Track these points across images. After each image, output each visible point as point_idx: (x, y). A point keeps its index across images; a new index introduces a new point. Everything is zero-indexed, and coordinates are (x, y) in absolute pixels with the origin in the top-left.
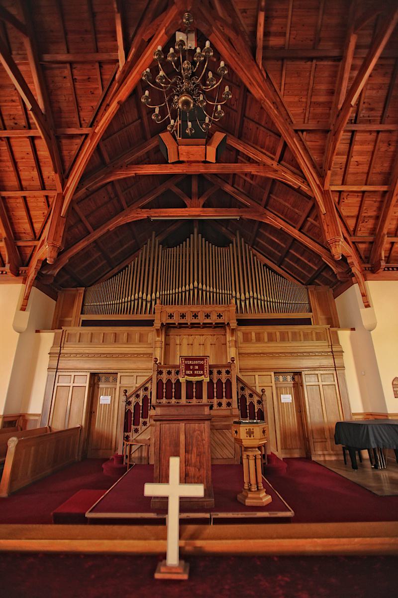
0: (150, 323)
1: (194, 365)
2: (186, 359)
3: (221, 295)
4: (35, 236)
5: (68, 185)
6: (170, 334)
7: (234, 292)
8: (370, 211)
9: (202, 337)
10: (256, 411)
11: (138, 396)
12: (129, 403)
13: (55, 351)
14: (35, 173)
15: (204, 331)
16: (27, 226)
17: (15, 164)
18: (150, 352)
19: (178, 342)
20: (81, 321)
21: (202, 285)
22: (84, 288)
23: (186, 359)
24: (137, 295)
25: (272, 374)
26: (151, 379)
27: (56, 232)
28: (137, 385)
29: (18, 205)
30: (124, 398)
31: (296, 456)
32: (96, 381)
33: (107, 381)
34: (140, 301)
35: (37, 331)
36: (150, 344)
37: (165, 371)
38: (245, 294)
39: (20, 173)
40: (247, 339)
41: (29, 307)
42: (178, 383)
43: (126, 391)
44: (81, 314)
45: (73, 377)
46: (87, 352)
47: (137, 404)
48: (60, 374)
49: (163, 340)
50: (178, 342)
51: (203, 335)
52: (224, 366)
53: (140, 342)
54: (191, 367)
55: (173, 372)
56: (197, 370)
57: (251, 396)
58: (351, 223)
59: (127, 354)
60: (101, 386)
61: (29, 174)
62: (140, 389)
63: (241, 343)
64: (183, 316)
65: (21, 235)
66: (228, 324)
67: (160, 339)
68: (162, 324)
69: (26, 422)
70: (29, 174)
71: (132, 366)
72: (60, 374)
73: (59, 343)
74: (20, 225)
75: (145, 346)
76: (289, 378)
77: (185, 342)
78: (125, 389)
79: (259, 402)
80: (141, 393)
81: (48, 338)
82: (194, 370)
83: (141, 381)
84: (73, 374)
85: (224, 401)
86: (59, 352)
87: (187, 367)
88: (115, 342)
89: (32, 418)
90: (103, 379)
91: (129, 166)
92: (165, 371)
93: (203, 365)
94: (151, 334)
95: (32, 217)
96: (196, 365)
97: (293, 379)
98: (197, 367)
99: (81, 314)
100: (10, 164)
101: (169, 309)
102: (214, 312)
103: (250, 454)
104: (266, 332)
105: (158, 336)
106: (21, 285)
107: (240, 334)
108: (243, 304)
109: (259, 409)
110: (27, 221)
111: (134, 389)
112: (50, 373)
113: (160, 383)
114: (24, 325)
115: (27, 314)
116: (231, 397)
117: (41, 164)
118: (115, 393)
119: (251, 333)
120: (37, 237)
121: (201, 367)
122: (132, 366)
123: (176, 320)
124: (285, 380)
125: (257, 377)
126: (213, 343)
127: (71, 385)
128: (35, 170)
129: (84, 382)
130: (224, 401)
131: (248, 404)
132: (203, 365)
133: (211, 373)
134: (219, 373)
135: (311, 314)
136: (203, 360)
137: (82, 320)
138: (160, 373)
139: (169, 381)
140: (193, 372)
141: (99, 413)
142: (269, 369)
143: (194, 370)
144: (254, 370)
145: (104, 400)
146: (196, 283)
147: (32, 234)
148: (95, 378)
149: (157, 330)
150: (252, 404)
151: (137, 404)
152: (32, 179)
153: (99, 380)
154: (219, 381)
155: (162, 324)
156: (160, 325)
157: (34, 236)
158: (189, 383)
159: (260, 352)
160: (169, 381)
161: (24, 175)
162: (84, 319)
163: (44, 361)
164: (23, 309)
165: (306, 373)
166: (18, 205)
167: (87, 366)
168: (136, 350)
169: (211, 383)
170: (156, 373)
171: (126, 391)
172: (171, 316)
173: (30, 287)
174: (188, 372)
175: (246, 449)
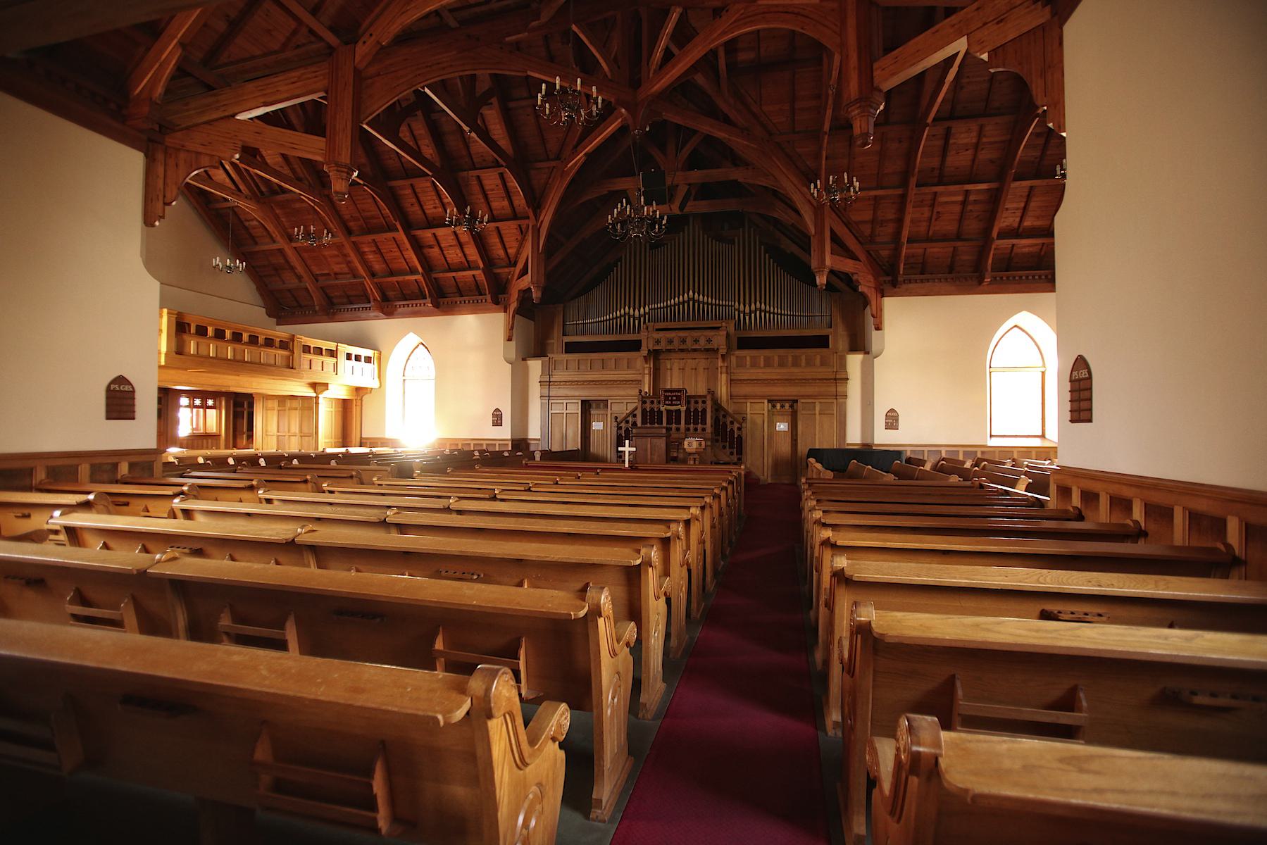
0: (635, 346)
1: (672, 397)
2: (665, 391)
3: (714, 307)
4: (510, 262)
5: (541, 218)
6: (660, 358)
7: (737, 303)
8: (890, 214)
9: (694, 361)
10: (736, 436)
11: (627, 422)
12: (619, 428)
13: (545, 380)
14: (506, 203)
15: (695, 355)
16: (501, 252)
17: (486, 196)
18: (639, 379)
19: (669, 367)
20: (564, 343)
21: (699, 296)
22: (562, 305)
23: (665, 391)
24: (622, 310)
25: (766, 401)
26: (636, 408)
27: (538, 272)
28: (628, 412)
29: (491, 233)
30: (615, 424)
31: (786, 482)
32: (587, 407)
33: (598, 407)
34: (627, 317)
35: (524, 359)
36: (639, 370)
37: (648, 401)
38: (750, 306)
39: (491, 203)
40: (741, 364)
41: (514, 338)
42: (660, 412)
43: (616, 418)
44: (563, 335)
45: (565, 404)
46: (576, 379)
47: (627, 429)
48: (553, 401)
49: (652, 366)
50: (669, 367)
51: (695, 359)
52: (700, 397)
53: (628, 368)
54: (670, 398)
55: (655, 402)
56: (674, 400)
57: (732, 423)
58: (867, 230)
59: (616, 381)
60: (592, 412)
61: (500, 204)
62: (629, 416)
63: (734, 369)
64: (670, 341)
65: (496, 261)
66: (718, 349)
67: (648, 366)
68: (649, 350)
69: (528, 445)
70: (500, 204)
71: (622, 393)
72: (553, 401)
73: (548, 371)
74: (494, 252)
75: (634, 372)
76: (787, 405)
77: (676, 367)
78: (616, 415)
79: (739, 429)
80: (630, 419)
81: (535, 366)
82: (672, 401)
83: (631, 407)
84: (565, 402)
85: (700, 426)
86: (548, 380)
87: (666, 398)
88: (603, 368)
89: (532, 442)
90: (594, 405)
91: (617, 675)
92: (648, 401)
93: (680, 396)
94: (638, 358)
95: (503, 236)
96: (674, 396)
97: (791, 406)
98: (675, 398)
99: (563, 335)
100: (481, 196)
101: (657, 335)
102: (702, 337)
103: (692, 457)
104: (762, 357)
105: (646, 363)
106: (502, 315)
107: (733, 359)
108: (747, 318)
109: (739, 435)
110: (501, 247)
111: (625, 415)
112: (543, 401)
113: (644, 411)
114: (513, 355)
115: (513, 343)
116: (706, 424)
117: (511, 194)
118: (607, 420)
119: (745, 357)
120: (513, 262)
121: (679, 398)
122: (622, 393)
123: (663, 346)
124: (782, 406)
125: (748, 404)
126: (706, 367)
127: (565, 412)
128: (506, 200)
129: (576, 408)
130: (700, 426)
131: (728, 430)
132: (680, 396)
133: (688, 403)
134: (696, 402)
135: (830, 330)
136: (678, 392)
137: (566, 343)
138: (644, 402)
139: (652, 409)
140: (672, 402)
141: (593, 438)
142: (763, 397)
143: (672, 401)
144: (746, 397)
145: (597, 426)
146: (691, 293)
147: (506, 259)
148: (586, 406)
149: (645, 357)
150: (732, 431)
151: (627, 429)
152: (503, 208)
153: (590, 406)
154: (696, 410)
155: (649, 350)
156: (647, 352)
157: (508, 262)
158: (668, 411)
159: (754, 378)
160: (652, 409)
161: (495, 205)
162: (567, 341)
163: (535, 391)
164: (510, 339)
165: (803, 401)
166: (491, 233)
167: (577, 393)
168: (625, 377)
169: (688, 410)
170: (641, 402)
171: (616, 418)
172: (658, 342)
173: (513, 317)
174: (667, 402)
175: (690, 454)
